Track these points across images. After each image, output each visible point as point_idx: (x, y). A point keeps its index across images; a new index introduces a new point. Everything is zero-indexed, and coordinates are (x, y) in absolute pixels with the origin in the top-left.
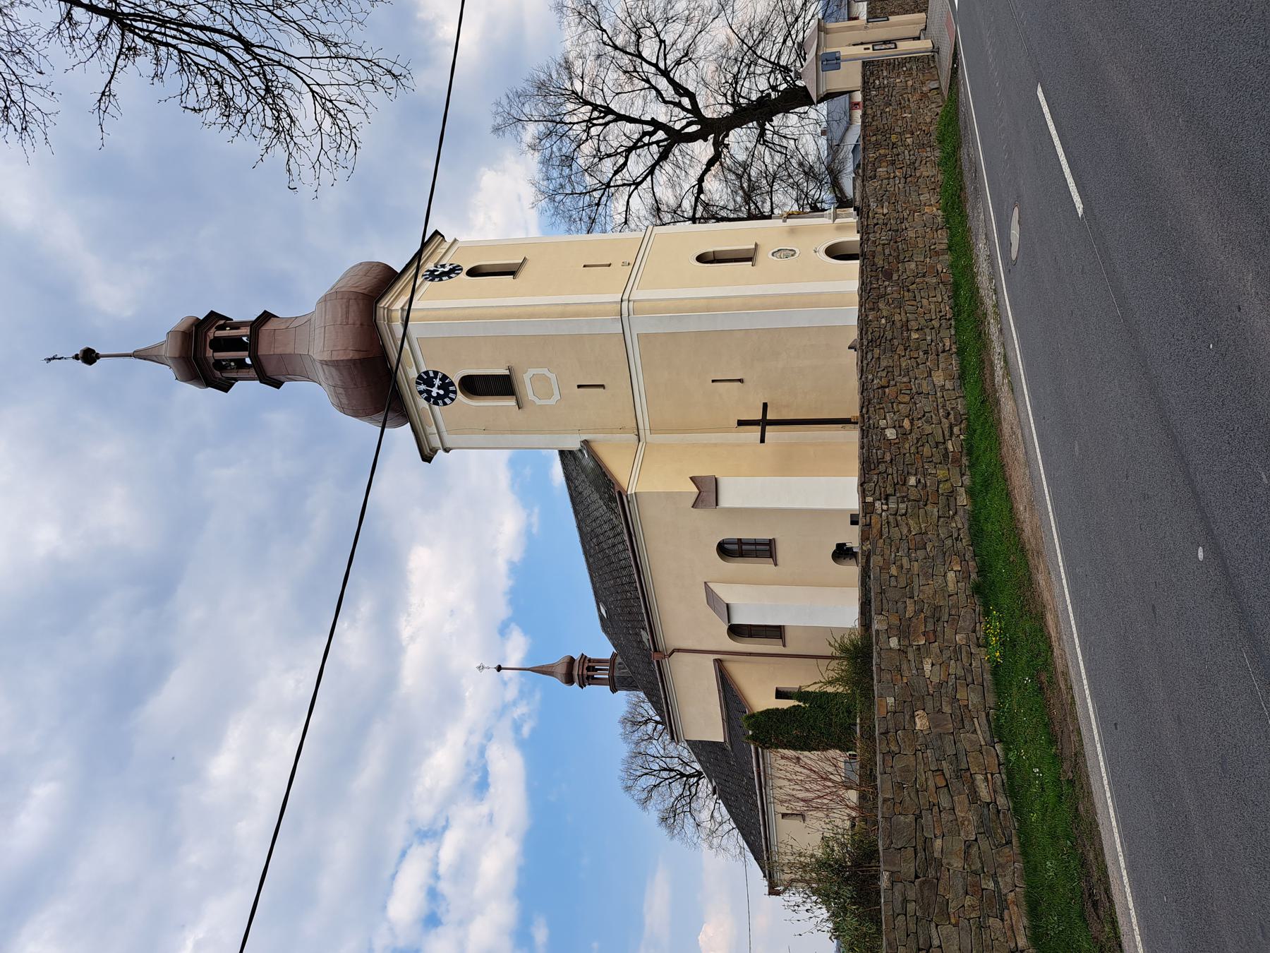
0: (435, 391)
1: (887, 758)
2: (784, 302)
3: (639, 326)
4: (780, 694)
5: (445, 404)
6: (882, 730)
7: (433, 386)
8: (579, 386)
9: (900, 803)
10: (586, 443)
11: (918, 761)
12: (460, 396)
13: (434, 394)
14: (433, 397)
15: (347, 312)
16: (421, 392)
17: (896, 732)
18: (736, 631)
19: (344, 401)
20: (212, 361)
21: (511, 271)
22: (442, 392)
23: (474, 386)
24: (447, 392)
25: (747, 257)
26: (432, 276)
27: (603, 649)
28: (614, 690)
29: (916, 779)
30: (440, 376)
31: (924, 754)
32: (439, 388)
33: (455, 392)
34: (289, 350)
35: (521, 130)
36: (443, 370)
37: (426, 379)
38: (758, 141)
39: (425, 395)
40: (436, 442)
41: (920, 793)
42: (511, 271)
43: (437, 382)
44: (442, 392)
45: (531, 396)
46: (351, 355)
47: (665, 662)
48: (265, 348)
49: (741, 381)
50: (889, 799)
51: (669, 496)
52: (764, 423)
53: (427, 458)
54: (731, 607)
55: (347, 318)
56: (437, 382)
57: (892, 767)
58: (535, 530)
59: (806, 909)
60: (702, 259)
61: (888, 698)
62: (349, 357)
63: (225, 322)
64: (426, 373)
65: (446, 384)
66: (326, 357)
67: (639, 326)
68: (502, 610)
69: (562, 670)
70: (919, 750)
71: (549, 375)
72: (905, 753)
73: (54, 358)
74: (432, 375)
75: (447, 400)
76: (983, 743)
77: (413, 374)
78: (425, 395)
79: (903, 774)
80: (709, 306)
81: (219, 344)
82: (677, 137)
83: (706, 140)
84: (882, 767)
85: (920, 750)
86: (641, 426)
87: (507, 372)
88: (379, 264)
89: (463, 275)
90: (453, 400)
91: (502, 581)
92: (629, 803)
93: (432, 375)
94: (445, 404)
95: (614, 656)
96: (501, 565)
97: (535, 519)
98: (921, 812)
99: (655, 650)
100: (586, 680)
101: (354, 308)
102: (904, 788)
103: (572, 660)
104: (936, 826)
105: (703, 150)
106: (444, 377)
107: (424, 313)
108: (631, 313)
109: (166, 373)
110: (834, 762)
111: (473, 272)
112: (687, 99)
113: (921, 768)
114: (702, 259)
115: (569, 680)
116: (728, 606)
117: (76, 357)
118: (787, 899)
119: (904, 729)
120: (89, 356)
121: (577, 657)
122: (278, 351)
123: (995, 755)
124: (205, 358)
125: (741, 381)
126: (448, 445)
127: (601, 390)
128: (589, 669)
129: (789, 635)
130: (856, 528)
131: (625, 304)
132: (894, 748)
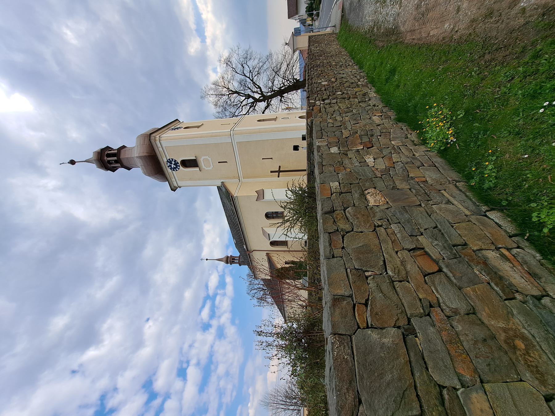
0: (173, 166)
1: (334, 238)
2: (285, 130)
4: (286, 263)
5: (177, 170)
6: (326, 209)
7: (172, 164)
8: (219, 162)
9: (366, 305)
10: (222, 182)
11: (381, 238)
12: (181, 168)
13: (173, 167)
14: (173, 168)
16: (168, 167)
17: (344, 210)
18: (273, 243)
20: (107, 161)
22: (175, 166)
24: (177, 166)
27: (237, 254)
28: (240, 265)
29: (384, 261)
30: (174, 160)
31: (388, 230)
32: (174, 165)
33: (179, 166)
34: (130, 156)
36: (175, 158)
37: (170, 161)
39: (170, 167)
41: (397, 284)
43: (173, 163)
44: (175, 166)
45: (204, 167)
46: (145, 154)
47: (251, 254)
48: (122, 156)
49: (271, 158)
50: (343, 297)
51: (248, 197)
52: (279, 171)
55: (144, 142)
56: (173, 163)
57: (343, 248)
59: (277, 358)
61: (331, 183)
63: (112, 149)
64: (169, 159)
65: (176, 164)
66: (137, 155)
67: (237, 139)
69: (225, 259)
70: (379, 226)
71: (209, 158)
72: (360, 230)
73: (63, 163)
74: (171, 160)
75: (177, 169)
76: (468, 213)
78: (170, 167)
79: (361, 256)
80: (260, 132)
81: (109, 155)
82: (256, 101)
83: (265, 102)
84: (328, 250)
85: (381, 226)
86: (240, 176)
87: (195, 158)
90: (179, 169)
94: (177, 170)
95: (240, 256)
98: (409, 320)
99: (248, 250)
102: (367, 278)
103: (228, 257)
104: (453, 353)
105: (263, 105)
106: (175, 161)
107: (166, 138)
108: (234, 134)
109: (94, 166)
113: (387, 247)
115: (227, 263)
116: (269, 234)
117: (69, 163)
118: (268, 351)
119: (354, 205)
120: (72, 162)
121: (229, 256)
122: (126, 157)
123: (494, 225)
124: (104, 160)
125: (271, 158)
128: (233, 259)
129: (289, 244)
130: (305, 142)
131: (232, 131)
132: (343, 225)
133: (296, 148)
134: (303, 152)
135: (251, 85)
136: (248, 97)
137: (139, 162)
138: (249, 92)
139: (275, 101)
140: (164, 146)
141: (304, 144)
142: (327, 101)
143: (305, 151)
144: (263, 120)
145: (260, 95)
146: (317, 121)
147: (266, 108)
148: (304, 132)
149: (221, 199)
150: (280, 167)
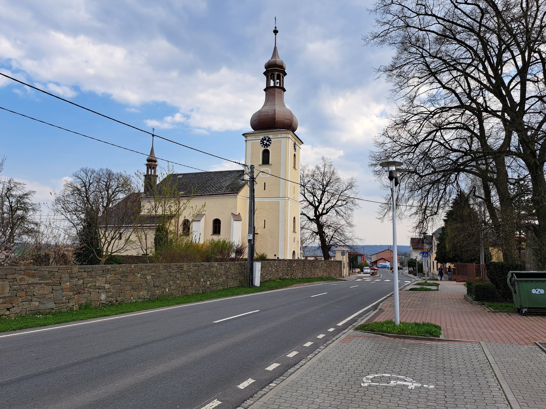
0: (265, 142)
2: (285, 240)
3: (281, 202)
5: (261, 144)
8: (265, 183)
12: (263, 149)
15: (288, 119)
19: (263, 114)
21: (294, 167)
22: (265, 144)
23: (266, 154)
24: (265, 145)
25: (294, 231)
26: (295, 144)
30: (270, 144)
32: (266, 143)
33: (264, 147)
35: (321, 166)
36: (271, 145)
38: (314, 231)
40: (249, 138)
42: (294, 167)
43: (268, 143)
44: (265, 144)
46: (276, 116)
49: (265, 227)
51: (236, 207)
53: (243, 135)
54: (200, 222)
56: (268, 143)
58: (127, 109)
60: (294, 217)
62: (276, 119)
64: (271, 140)
65: (267, 145)
67: (281, 202)
68: (87, 87)
74: (270, 142)
77: (271, 137)
80: (285, 221)
82: (316, 208)
83: (314, 216)
87: (270, 163)
88: (297, 127)
89: (294, 153)
90: (262, 146)
91: (100, 89)
92: (76, 169)
93: (270, 142)
94: (261, 144)
96: (110, 91)
97: (133, 110)
100: (149, 166)
101: (289, 121)
105: (311, 214)
106: (269, 145)
107: (288, 143)
110: (151, 252)
111: (295, 154)
112: (325, 212)
114: (294, 217)
117: (276, 35)
122: (276, 94)
125: (265, 227)
126: (248, 141)
127: (264, 189)
131: (288, 199)
133: (275, 255)
134: (273, 258)
135: (327, 206)
136: (320, 203)
137: (269, 108)
138: (323, 202)
139: (314, 226)
140: (282, 139)
141: (276, 258)
142: (287, 265)
143: (274, 258)
144: (294, 221)
145: (320, 212)
146: (282, 262)
147: (308, 218)
148: (280, 258)
149: (229, 172)
150: (258, 234)
